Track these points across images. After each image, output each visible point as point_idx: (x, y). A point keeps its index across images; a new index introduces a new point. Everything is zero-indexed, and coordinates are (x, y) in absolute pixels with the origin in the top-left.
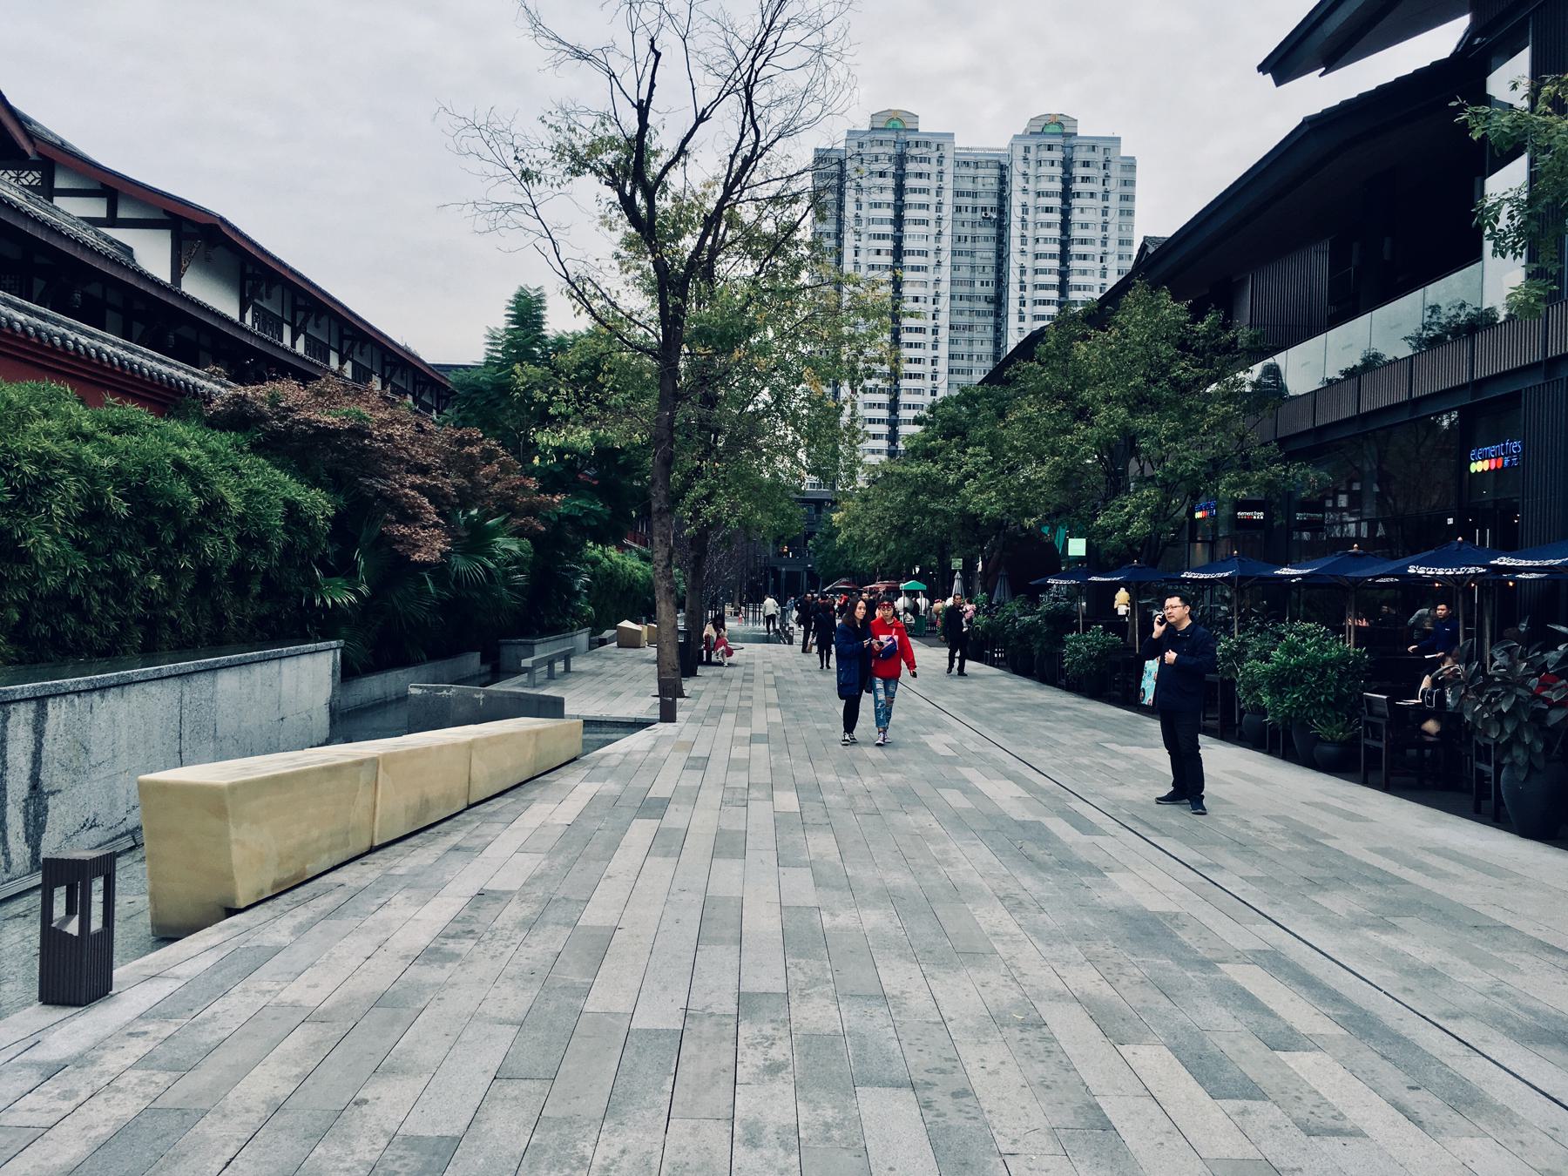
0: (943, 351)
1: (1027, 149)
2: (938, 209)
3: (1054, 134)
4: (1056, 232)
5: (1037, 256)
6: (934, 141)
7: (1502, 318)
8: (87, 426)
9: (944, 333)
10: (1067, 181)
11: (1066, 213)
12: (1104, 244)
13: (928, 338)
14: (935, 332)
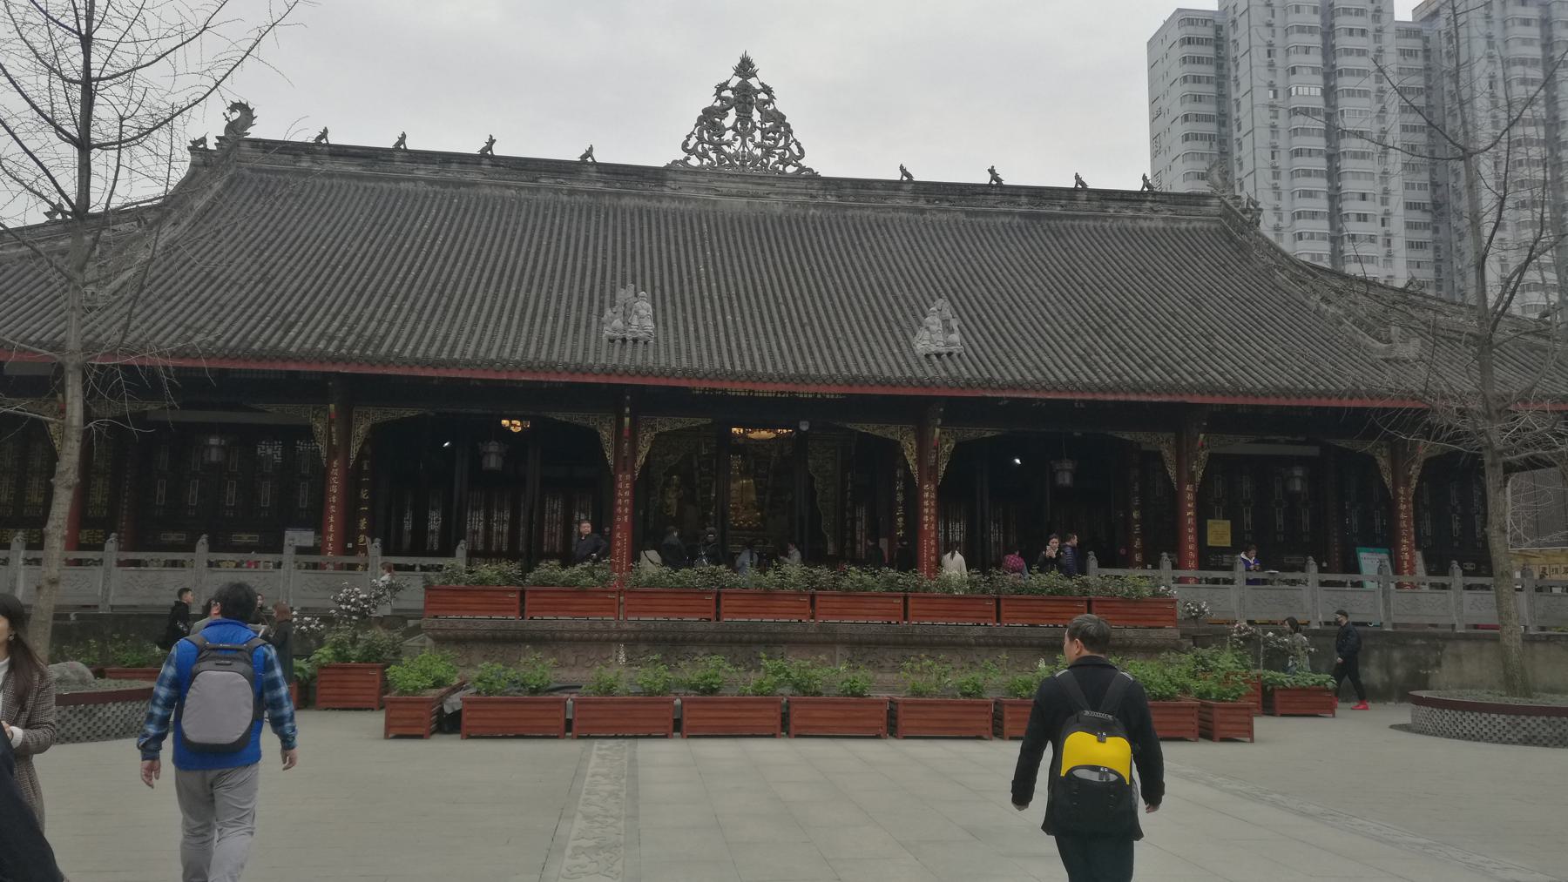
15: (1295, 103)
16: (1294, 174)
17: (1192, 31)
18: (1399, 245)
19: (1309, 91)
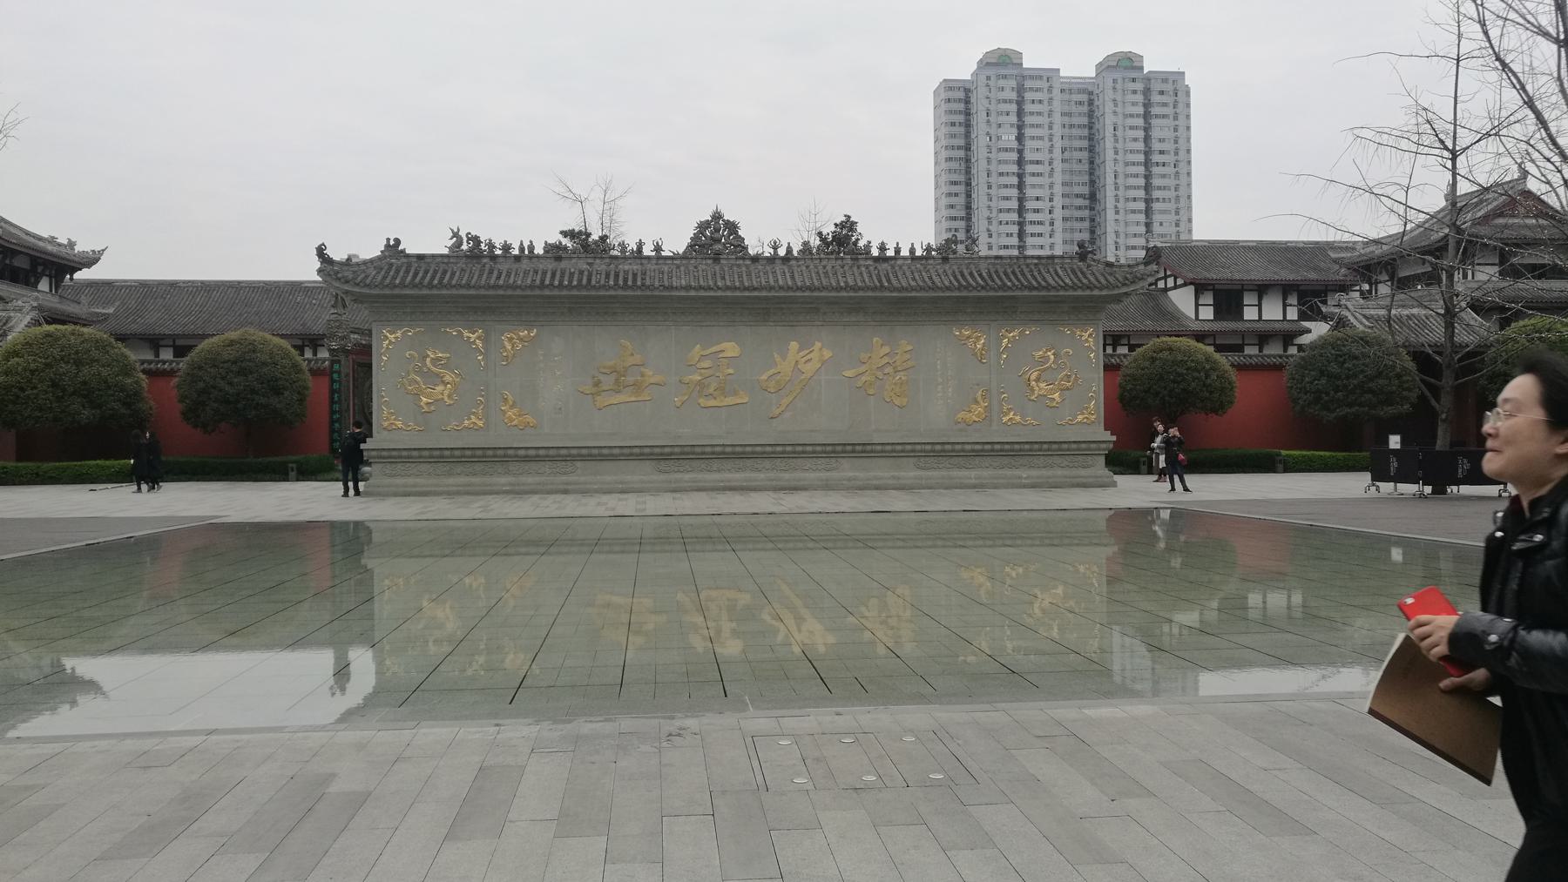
1: (1115, 81)
3: (1124, 64)
4: (1140, 146)
5: (1127, 164)
6: (1045, 75)
7: (69, 663)
8: (120, 344)
10: (1147, 105)
11: (1147, 129)
12: (1176, 154)
14: (1052, 224)
15: (1001, 145)
16: (1000, 186)
17: (951, 95)
18: (1059, 224)
19: (1009, 138)
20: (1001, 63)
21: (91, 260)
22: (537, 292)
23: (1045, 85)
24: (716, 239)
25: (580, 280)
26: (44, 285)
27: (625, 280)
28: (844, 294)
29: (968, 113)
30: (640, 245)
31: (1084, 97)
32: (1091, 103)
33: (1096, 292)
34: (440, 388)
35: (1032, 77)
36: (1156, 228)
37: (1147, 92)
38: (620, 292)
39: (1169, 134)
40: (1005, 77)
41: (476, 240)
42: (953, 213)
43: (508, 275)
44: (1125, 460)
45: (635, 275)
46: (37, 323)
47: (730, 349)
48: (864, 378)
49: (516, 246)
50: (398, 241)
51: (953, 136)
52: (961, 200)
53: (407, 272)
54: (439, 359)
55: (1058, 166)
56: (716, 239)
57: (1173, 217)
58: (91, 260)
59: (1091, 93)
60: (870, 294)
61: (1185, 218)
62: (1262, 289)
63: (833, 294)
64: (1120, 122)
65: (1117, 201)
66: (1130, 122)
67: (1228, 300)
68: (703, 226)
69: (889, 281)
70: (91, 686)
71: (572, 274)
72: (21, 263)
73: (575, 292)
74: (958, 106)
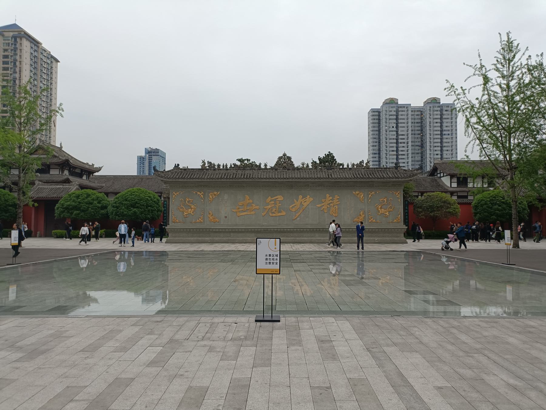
0: (410, 160)
1: (430, 107)
2: (407, 116)
6: (406, 106)
7: (88, 293)
9: (410, 156)
13: (405, 117)
14: (408, 155)
17: (374, 113)
20: (391, 102)
21: (99, 169)
22: (219, 180)
23: (406, 109)
24: (285, 163)
25: (233, 176)
26: (84, 177)
27: (247, 176)
28: (316, 180)
29: (379, 119)
30: (260, 164)
31: (419, 113)
32: (422, 114)
33: (400, 180)
34: (190, 210)
35: (401, 107)
36: (445, 156)
37: (441, 111)
38: (245, 180)
39: (449, 124)
40: (392, 107)
41: (210, 163)
42: (375, 152)
43: (211, 175)
44: (412, 234)
45: (250, 175)
46: (77, 189)
47: (280, 198)
48: (323, 207)
49: (222, 165)
50: (178, 165)
51: (374, 127)
52: (377, 148)
53: (181, 174)
54: (190, 201)
55: (410, 136)
56: (285, 163)
57: (450, 152)
58: (99, 169)
59: (421, 112)
60: (325, 180)
61: (454, 152)
62: (475, 177)
63: (313, 180)
64: (432, 121)
65: (431, 147)
66: (436, 121)
67: (462, 181)
68: (280, 158)
69: (331, 176)
70: (95, 301)
71: (231, 175)
72: (78, 171)
73: (231, 180)
74: (376, 116)
